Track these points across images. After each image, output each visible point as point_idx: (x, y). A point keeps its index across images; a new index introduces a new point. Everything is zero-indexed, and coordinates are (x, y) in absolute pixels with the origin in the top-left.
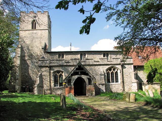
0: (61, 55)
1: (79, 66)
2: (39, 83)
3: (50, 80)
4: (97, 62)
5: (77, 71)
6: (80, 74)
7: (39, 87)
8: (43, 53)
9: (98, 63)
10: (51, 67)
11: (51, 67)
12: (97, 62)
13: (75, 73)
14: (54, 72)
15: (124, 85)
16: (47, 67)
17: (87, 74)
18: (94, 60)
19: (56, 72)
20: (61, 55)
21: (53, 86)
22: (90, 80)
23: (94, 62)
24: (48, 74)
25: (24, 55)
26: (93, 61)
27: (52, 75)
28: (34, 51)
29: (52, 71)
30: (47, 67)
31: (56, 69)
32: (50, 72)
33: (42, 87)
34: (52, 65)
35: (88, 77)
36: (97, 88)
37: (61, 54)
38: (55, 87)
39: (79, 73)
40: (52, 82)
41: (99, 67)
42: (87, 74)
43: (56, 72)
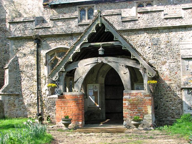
0: (87, 11)
1: (97, 28)
2: (8, 83)
3: (38, 75)
4: (176, 18)
5: (92, 44)
6: (100, 53)
7: (9, 95)
8: (42, 9)
9: (177, 23)
10: (39, 41)
11: (39, 41)
12: (176, 18)
13: (86, 53)
14: (50, 54)
15: (165, 29)
16: (29, 39)
17: (122, 53)
18: (165, 15)
19: (54, 54)
20: (87, 11)
21: (47, 93)
22: (136, 78)
23: (166, 19)
24: (32, 60)
25: (4, 17)
26: (163, 17)
27: (44, 61)
28: (25, 8)
29: (43, 53)
30: (29, 39)
31: (53, 45)
32: (38, 55)
33: (18, 95)
34: (41, 33)
35: (131, 63)
36: (175, 99)
37: (86, 9)
38: (52, 95)
39: (101, 49)
40: (43, 81)
41: (180, 34)
42: (122, 53)
43: (56, 55)
